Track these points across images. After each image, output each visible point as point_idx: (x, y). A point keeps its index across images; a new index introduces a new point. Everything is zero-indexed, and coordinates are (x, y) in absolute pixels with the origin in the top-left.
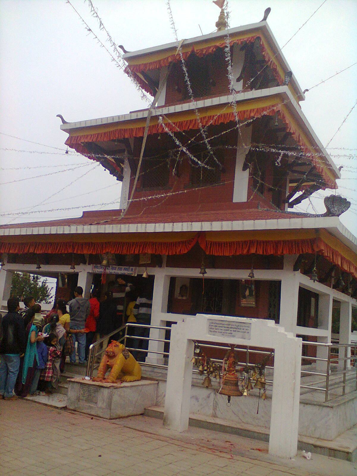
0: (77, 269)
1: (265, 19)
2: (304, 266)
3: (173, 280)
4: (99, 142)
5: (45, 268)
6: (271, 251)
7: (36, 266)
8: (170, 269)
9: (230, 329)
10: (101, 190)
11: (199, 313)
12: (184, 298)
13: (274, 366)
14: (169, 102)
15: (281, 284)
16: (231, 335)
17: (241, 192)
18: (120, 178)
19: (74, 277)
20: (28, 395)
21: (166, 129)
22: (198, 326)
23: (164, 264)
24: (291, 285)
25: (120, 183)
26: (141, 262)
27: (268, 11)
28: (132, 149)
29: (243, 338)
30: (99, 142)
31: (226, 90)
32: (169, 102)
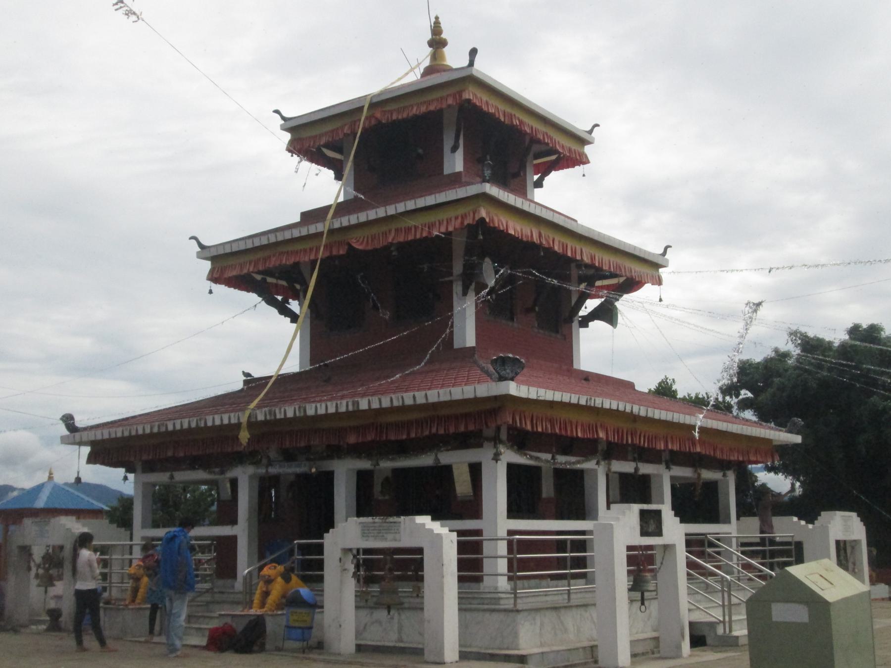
1: (471, 64)
4: (253, 267)
12: (387, 497)
17: (456, 162)
27: (473, 52)
29: (395, 540)
30: (253, 267)
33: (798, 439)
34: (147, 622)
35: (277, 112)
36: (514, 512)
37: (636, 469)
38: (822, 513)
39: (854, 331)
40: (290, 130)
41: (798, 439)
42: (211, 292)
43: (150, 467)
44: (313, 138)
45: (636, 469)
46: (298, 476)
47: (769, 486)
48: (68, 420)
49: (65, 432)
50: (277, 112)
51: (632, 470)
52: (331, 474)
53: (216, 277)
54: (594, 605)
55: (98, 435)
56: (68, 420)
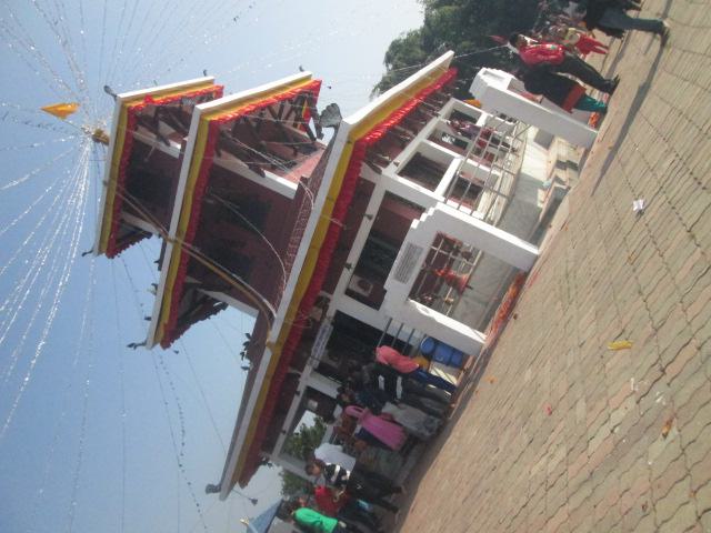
0: (301, 388)
2: (378, 163)
3: (349, 293)
4: (185, 306)
5: (286, 426)
6: (354, 192)
7: (345, 270)
8: (337, 289)
9: (408, 264)
10: (232, 324)
11: (383, 283)
12: (372, 287)
13: (466, 351)
14: (163, 222)
15: (313, 389)
16: (414, 264)
18: (224, 306)
19: (312, 393)
20: (423, 30)
21: (566, 15)
22: (396, 287)
23: (329, 296)
24: (392, 177)
25: (229, 308)
26: (318, 319)
28: (196, 281)
29: (420, 253)
30: (185, 306)
31: (176, 163)
32: (163, 222)
33: (450, 54)
34: (654, 88)
35: (84, 254)
36: (432, 185)
37: (349, 267)
38: (470, 91)
39: (389, 59)
40: (100, 252)
41: (450, 54)
42: (177, 352)
43: (268, 446)
44: (117, 238)
45: (349, 267)
46: (328, 347)
47: (423, 154)
48: (211, 489)
49: (217, 494)
50: (84, 254)
51: (348, 261)
52: (339, 314)
53: (166, 344)
54: (391, 319)
55: (229, 477)
56: (211, 489)
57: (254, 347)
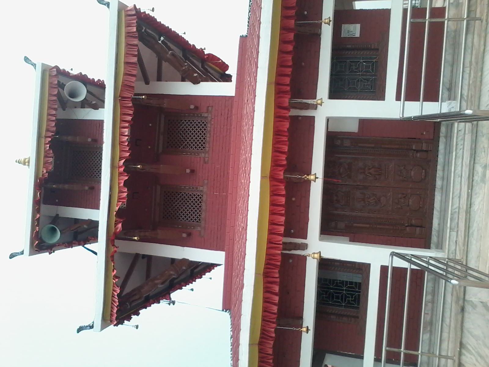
4: (133, 292)
30: (133, 292)
57: (231, 302)
